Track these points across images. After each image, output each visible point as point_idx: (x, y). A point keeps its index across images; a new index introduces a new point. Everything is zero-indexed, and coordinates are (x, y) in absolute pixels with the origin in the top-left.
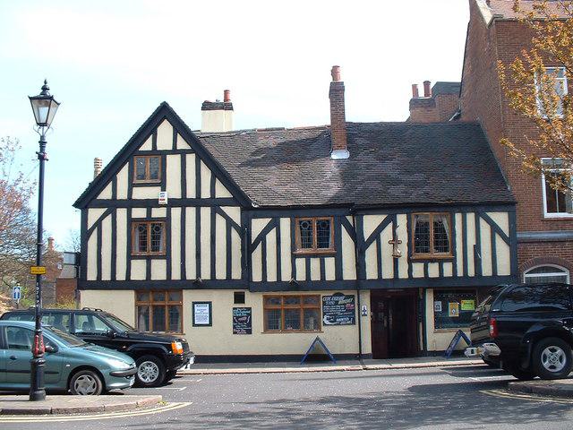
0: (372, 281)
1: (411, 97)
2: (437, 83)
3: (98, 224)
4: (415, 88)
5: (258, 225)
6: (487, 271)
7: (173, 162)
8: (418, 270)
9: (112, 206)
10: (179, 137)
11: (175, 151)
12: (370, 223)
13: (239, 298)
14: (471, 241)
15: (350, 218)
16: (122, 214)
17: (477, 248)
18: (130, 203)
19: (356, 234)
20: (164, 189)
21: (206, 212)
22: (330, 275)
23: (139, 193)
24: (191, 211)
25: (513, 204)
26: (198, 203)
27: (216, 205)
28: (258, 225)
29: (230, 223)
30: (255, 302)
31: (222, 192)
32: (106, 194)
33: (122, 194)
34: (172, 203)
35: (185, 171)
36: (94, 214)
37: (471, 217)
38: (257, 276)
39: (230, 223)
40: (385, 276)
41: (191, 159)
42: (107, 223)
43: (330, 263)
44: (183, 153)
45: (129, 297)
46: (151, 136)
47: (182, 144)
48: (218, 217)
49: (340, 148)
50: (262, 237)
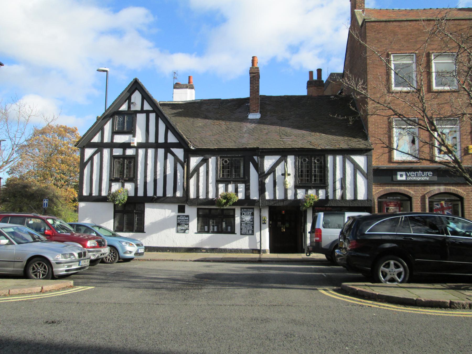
0: (269, 200)
1: (308, 80)
2: (332, 75)
3: (91, 158)
4: (311, 73)
5: (194, 161)
6: (349, 196)
7: (141, 118)
8: (301, 194)
9: (100, 146)
10: (145, 102)
11: (142, 111)
12: (268, 162)
13: (181, 209)
14: (339, 175)
15: (255, 158)
16: (106, 152)
17: (343, 180)
18: (112, 145)
19: (259, 167)
20: (134, 136)
21: (161, 152)
22: (241, 196)
23: (119, 139)
24: (151, 152)
25: (370, 150)
26: (156, 146)
27: (167, 147)
28: (194, 161)
29: (176, 159)
30: (191, 211)
31: (172, 139)
32: (96, 139)
33: (107, 140)
34: (140, 146)
35: (333, 169)
36: (89, 152)
37: (339, 159)
38: (192, 195)
39: (176, 159)
40: (201, 197)
41: (152, 116)
42: (96, 158)
43: (241, 187)
44: (148, 112)
45: (108, 208)
46: (366, 172)
47: (147, 107)
48: (169, 155)
49: (255, 111)
50: (197, 170)
